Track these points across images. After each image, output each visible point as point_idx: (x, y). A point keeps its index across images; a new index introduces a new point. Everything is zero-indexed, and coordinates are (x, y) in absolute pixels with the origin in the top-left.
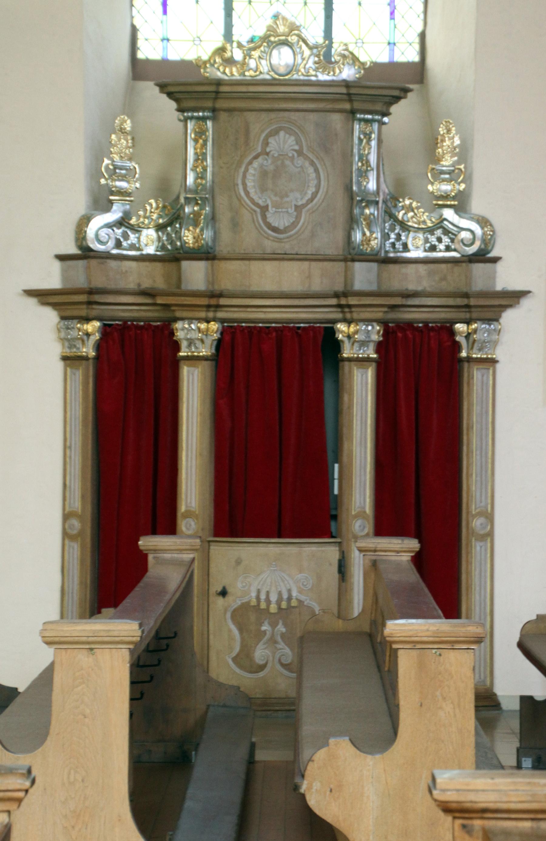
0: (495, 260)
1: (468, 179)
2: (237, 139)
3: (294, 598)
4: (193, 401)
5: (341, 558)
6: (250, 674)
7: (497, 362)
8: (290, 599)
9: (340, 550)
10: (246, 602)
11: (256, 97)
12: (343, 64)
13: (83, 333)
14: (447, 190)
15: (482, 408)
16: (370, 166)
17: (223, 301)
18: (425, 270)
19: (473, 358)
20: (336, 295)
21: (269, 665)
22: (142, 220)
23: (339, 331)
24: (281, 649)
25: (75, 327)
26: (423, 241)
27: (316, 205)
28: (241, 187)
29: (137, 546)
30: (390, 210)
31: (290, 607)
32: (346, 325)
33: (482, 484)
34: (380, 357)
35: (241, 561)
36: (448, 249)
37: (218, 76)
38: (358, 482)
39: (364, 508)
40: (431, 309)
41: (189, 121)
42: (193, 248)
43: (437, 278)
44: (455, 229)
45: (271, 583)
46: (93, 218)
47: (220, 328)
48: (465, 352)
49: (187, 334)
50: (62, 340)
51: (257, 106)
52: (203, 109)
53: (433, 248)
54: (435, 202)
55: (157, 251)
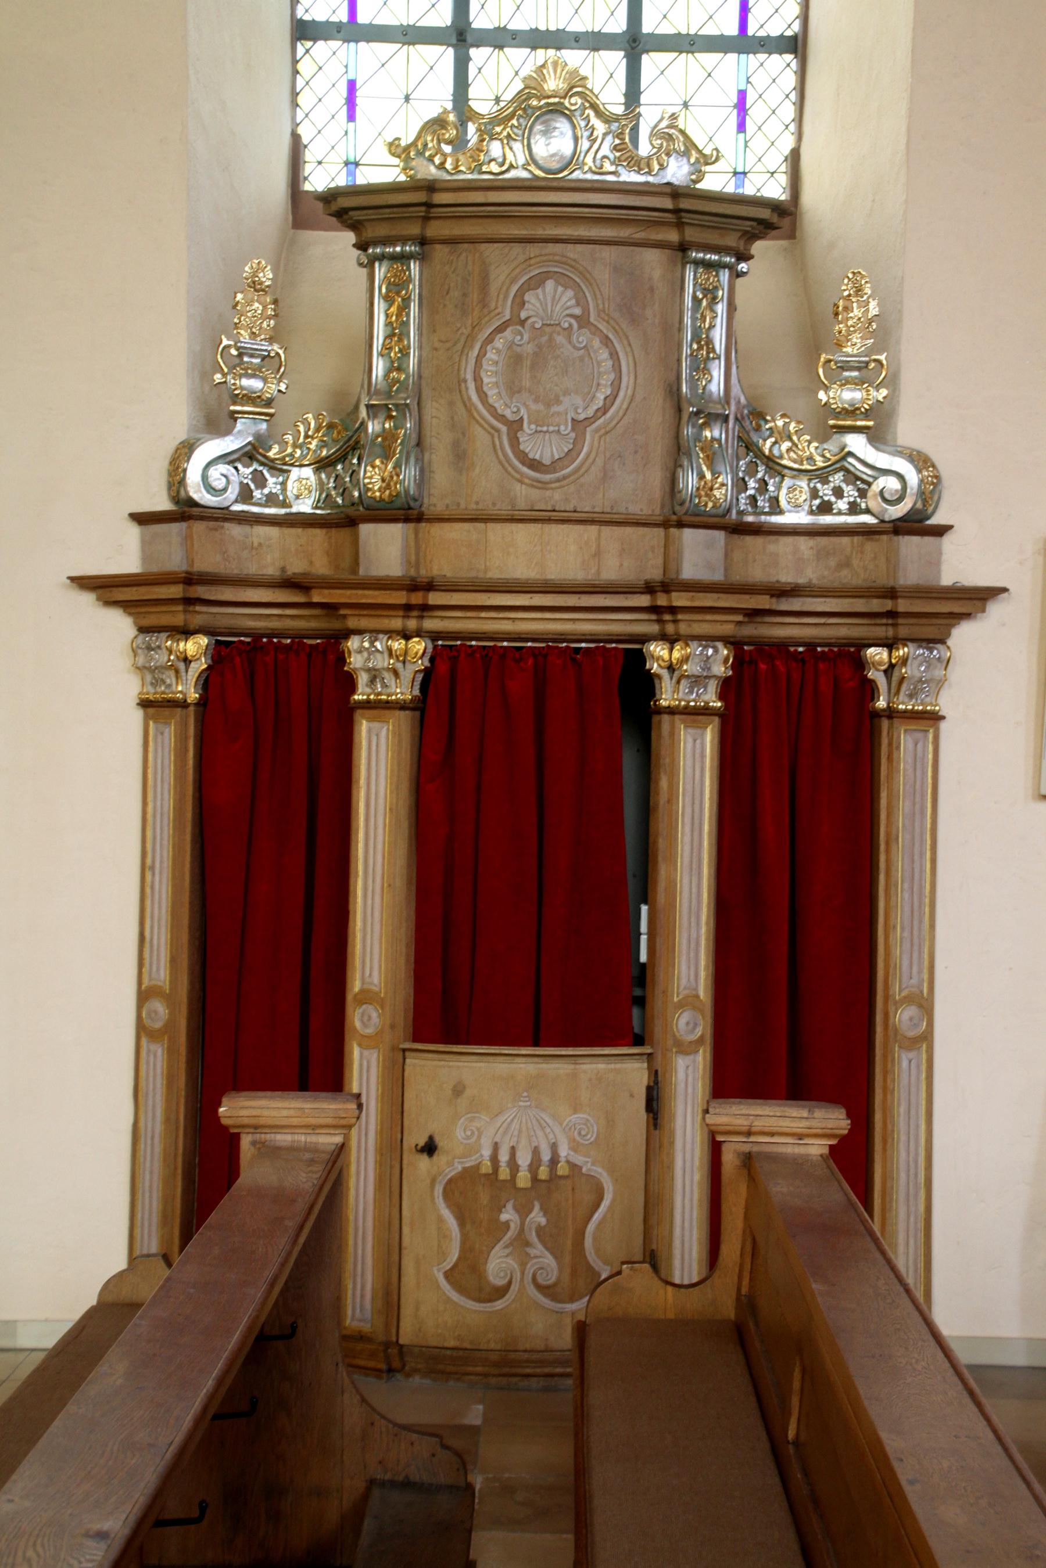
0: (940, 531)
1: (892, 382)
2: (465, 295)
3: (563, 1160)
4: (377, 786)
5: (652, 1084)
6: (477, 1304)
7: (943, 718)
8: (554, 1161)
9: (649, 1068)
10: (472, 1167)
11: (502, 213)
12: (668, 155)
13: (177, 657)
14: (853, 399)
15: (914, 804)
16: (714, 350)
17: (435, 598)
18: (812, 548)
19: (898, 711)
20: (649, 589)
21: (514, 1288)
22: (289, 450)
23: (653, 656)
24: (536, 1257)
25: (163, 646)
26: (808, 494)
27: (612, 419)
28: (472, 385)
29: (217, 1118)
30: (749, 435)
31: (554, 1177)
32: (665, 646)
33: (912, 945)
34: (726, 707)
35: (464, 1087)
36: (854, 509)
37: (432, 175)
38: (684, 942)
39: (696, 989)
40: (822, 620)
41: (377, 265)
42: (381, 500)
43: (832, 562)
44: (869, 472)
45: (520, 1132)
46: (198, 446)
47: (430, 650)
48: (884, 700)
49: (368, 659)
50: (140, 669)
51: (504, 232)
52: (404, 240)
53: (826, 508)
54: (831, 422)
55: (317, 508)
